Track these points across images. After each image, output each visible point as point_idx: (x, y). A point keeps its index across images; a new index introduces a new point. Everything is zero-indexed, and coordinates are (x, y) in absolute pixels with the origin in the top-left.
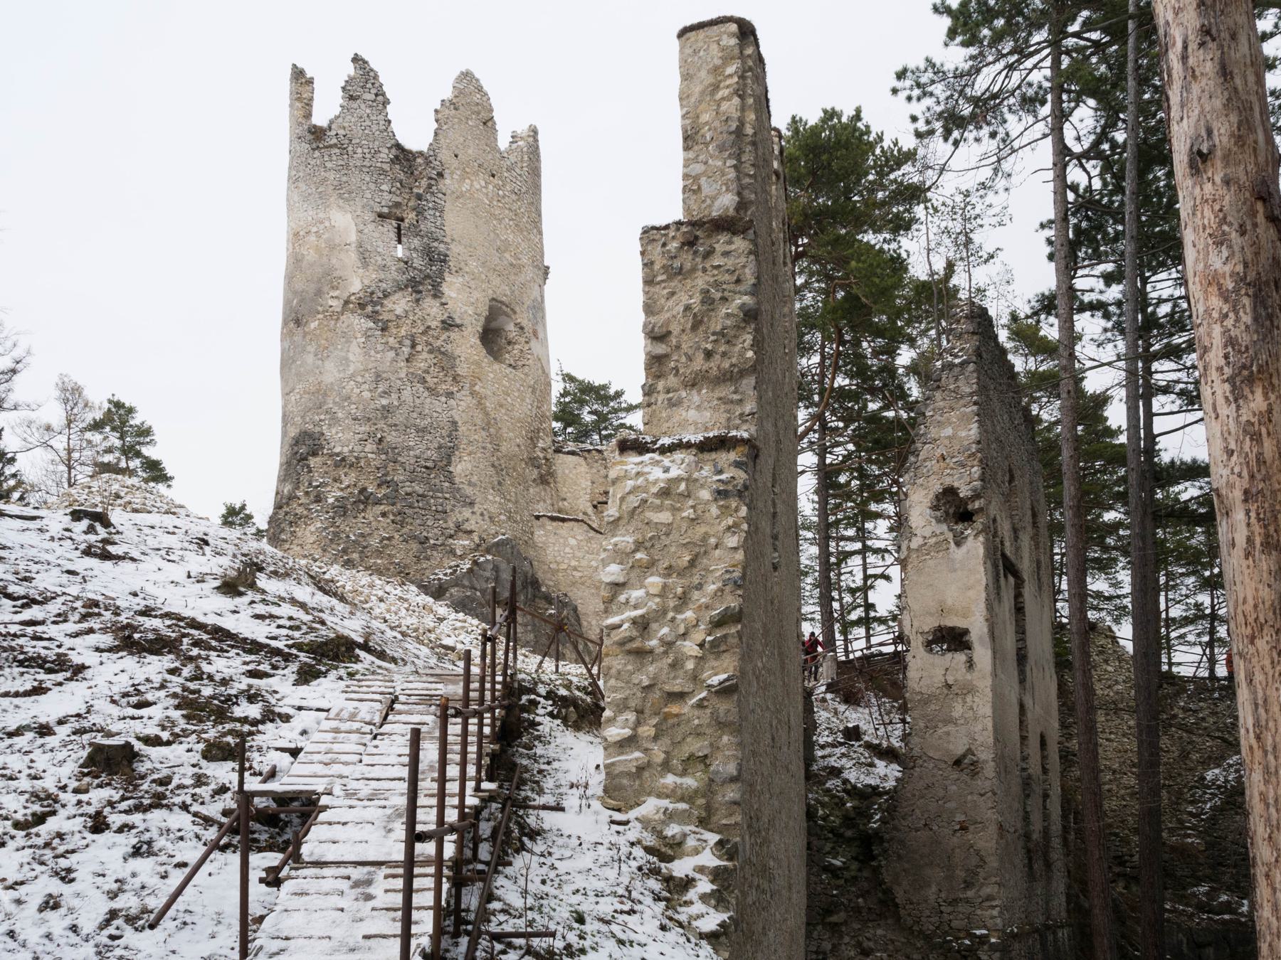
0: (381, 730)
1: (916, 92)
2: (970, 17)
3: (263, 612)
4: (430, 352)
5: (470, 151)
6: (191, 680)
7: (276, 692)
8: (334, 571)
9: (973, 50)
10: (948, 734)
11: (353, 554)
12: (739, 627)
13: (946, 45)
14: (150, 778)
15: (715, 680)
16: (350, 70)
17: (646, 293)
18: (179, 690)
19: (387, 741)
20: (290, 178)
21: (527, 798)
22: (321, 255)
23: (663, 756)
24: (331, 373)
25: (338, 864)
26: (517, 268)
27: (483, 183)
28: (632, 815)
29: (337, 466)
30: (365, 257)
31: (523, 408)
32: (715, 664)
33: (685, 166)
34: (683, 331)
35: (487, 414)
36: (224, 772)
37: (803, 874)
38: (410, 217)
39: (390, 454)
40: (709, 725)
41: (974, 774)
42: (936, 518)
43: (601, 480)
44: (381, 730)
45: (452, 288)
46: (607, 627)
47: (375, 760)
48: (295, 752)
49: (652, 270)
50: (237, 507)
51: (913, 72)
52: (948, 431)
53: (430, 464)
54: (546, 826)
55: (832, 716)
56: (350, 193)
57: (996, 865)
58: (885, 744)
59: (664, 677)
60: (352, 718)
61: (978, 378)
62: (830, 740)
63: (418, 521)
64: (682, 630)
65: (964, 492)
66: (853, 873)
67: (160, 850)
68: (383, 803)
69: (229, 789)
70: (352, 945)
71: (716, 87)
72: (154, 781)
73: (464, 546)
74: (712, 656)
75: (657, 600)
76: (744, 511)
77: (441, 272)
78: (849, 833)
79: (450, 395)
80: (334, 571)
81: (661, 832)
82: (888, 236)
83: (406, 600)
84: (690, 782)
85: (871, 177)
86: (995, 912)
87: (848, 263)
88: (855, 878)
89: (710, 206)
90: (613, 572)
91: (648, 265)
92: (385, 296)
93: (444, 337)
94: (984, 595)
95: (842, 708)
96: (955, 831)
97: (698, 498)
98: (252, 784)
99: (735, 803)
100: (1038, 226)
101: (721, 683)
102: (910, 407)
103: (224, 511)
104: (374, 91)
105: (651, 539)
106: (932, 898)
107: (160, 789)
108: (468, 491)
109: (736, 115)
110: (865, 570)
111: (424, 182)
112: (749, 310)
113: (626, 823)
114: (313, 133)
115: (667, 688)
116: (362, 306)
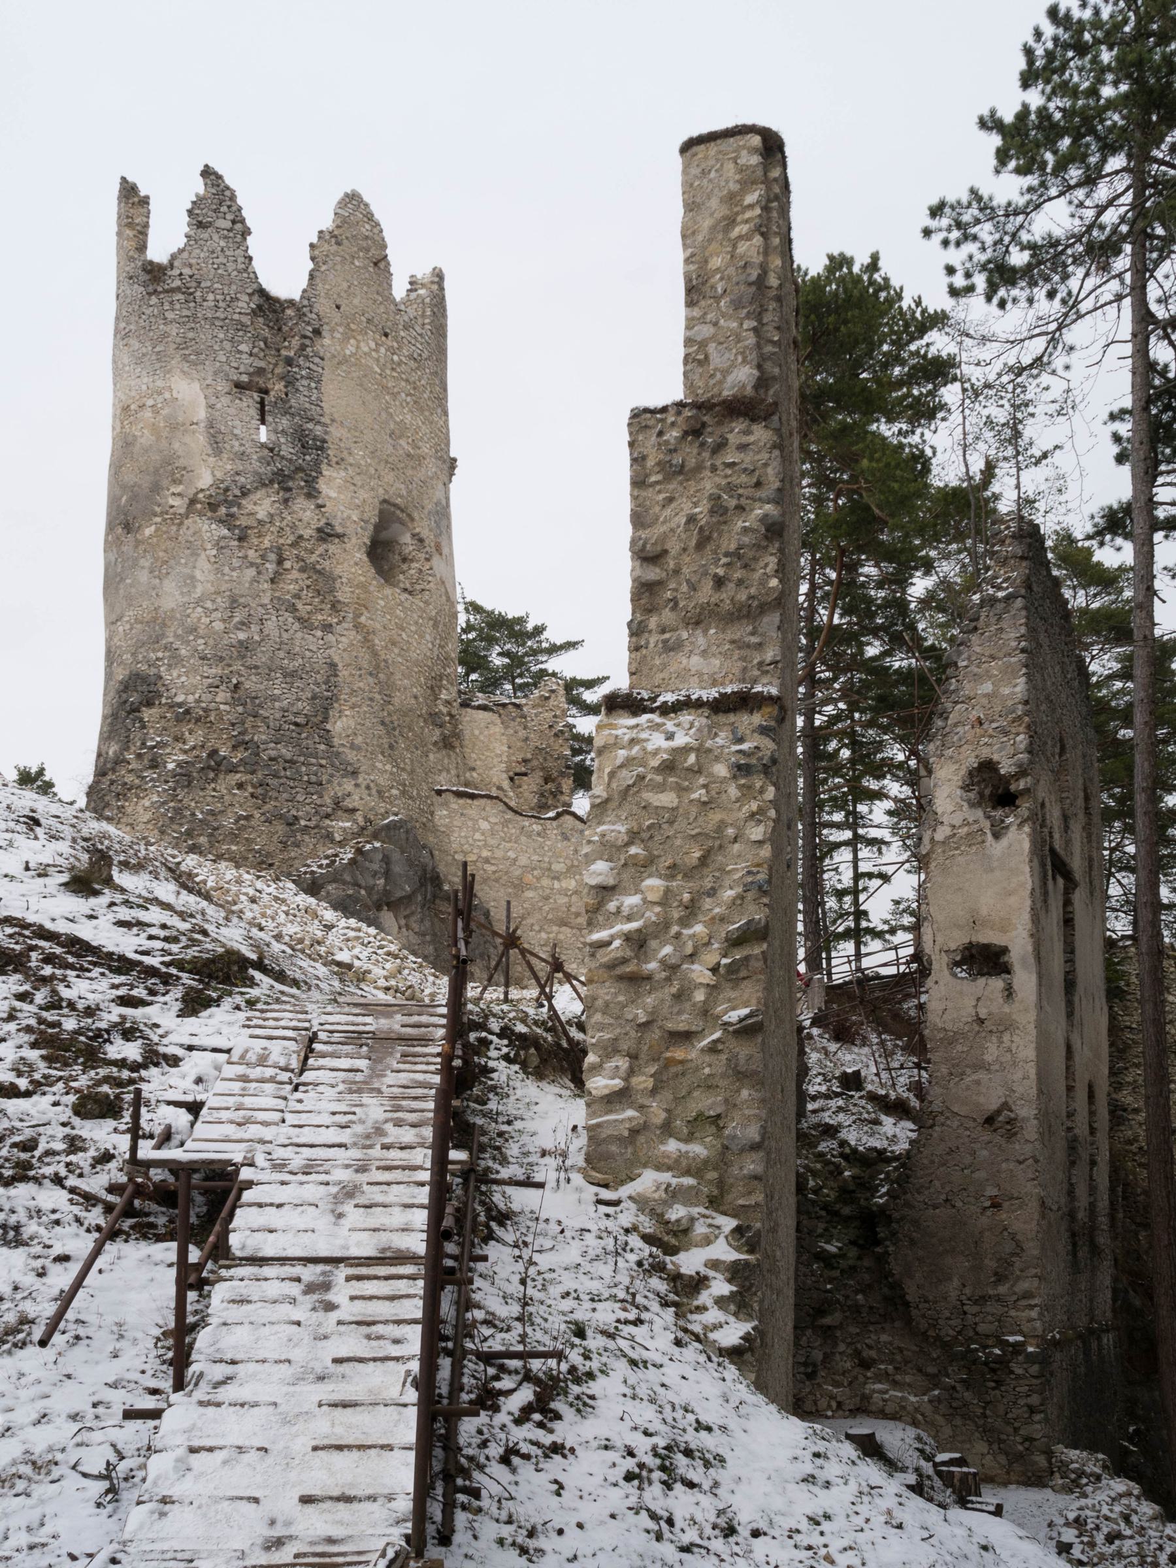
0: (303, 1079)
1: (955, 234)
2: (1027, 135)
3: (128, 918)
4: (302, 570)
5: (356, 301)
6: (47, 1008)
7: (157, 1026)
8: (190, 862)
9: (1032, 180)
10: (978, 1083)
11: (202, 836)
12: (765, 946)
13: (998, 172)
14: (9, 1142)
15: (733, 1016)
16: (198, 186)
17: (634, 498)
18: (33, 1022)
19: (312, 1094)
20: (117, 331)
21: (488, 1170)
22: (159, 438)
23: (663, 1115)
24: (171, 596)
25: (283, 1260)
26: (416, 459)
27: (373, 345)
28: (624, 1192)
29: (179, 719)
30: (216, 441)
31: (422, 646)
32: (733, 994)
33: (688, 328)
34: (685, 550)
35: (375, 654)
36: (104, 1134)
37: (792, 1259)
38: (278, 387)
39: (249, 706)
40: (724, 1076)
41: (1011, 1135)
42: (969, 801)
43: (519, 744)
44: (303, 1079)
45: (332, 484)
46: (591, 945)
47: (303, 1119)
48: (194, 1108)
49: (644, 467)
50: (33, 771)
51: (953, 208)
52: (987, 687)
54: (516, 1207)
55: (829, 1059)
56: (198, 354)
57: (1036, 1252)
58: (893, 1096)
59: (665, 1011)
60: (262, 1061)
61: (1027, 618)
62: (823, 1089)
63: (285, 795)
64: (689, 950)
65: (1006, 768)
66: (851, 1262)
67: (32, 1238)
68: (323, 1178)
69: (113, 1156)
70: (319, 1370)
71: (731, 222)
72: (14, 1145)
73: (344, 829)
74: (729, 985)
75: (658, 909)
76: (771, 793)
77: (317, 464)
78: (846, 1211)
79: (327, 628)
80: (190, 862)
81: (662, 1215)
82: (904, 427)
83: (284, 901)
84: (698, 1150)
85: (885, 348)
86: (1034, 1314)
87: (857, 461)
88: (853, 1268)
89: (721, 382)
90: (600, 871)
91: (638, 460)
92: (244, 494)
93: (320, 550)
94: (1028, 903)
95: (833, 1047)
96: (985, 1208)
97: (711, 775)
98: (146, 1151)
99: (756, 1178)
100: (1106, 416)
101: (741, 1020)
102: (932, 653)
104: (230, 217)
105: (649, 827)
106: (953, 1294)
107: (24, 1156)
108: (351, 756)
109: (757, 259)
110: (856, 867)
111: (296, 342)
112: (773, 524)
113: (616, 1203)
114: (149, 272)
115: (670, 1026)
116: (213, 507)
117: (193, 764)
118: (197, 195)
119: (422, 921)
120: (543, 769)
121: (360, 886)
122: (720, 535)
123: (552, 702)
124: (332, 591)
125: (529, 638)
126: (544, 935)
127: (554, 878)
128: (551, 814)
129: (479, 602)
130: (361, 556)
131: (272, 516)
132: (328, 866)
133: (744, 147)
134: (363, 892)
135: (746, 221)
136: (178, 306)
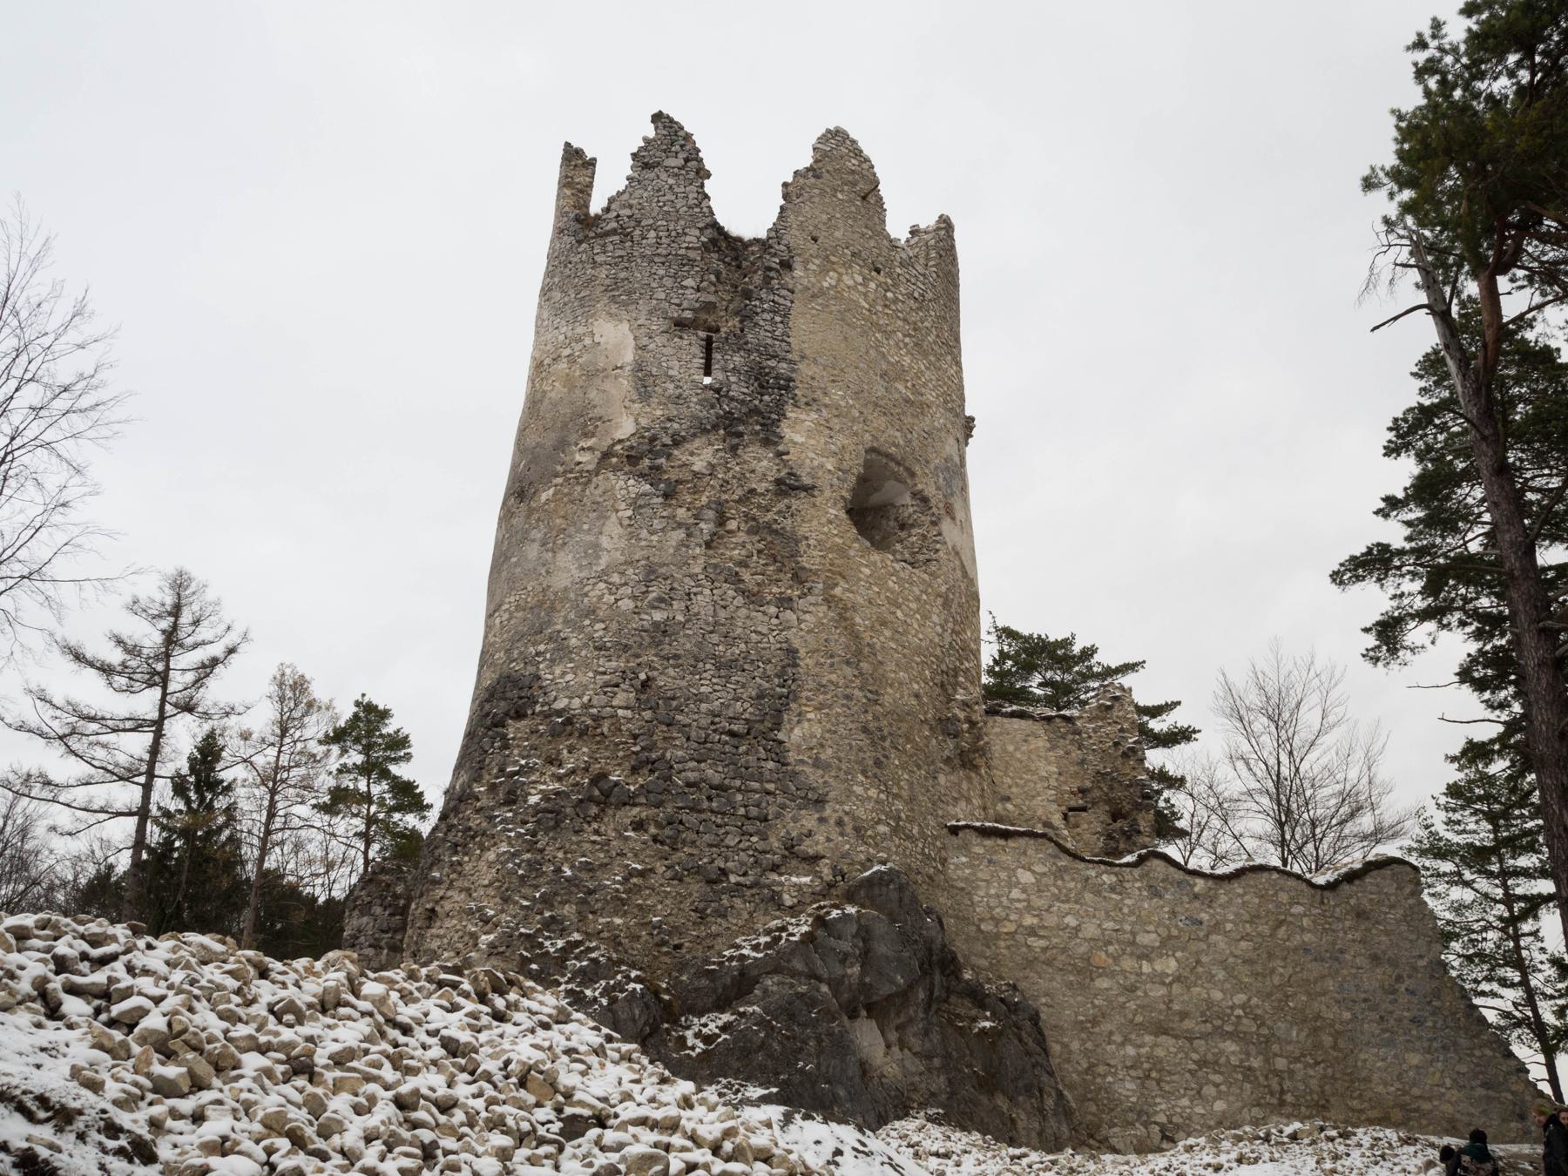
5: (837, 234)
24: (566, 570)
27: (859, 279)
29: (555, 734)
30: (644, 382)
35: (856, 636)
39: (662, 711)
45: (801, 432)
56: (629, 293)
73: (799, 887)
79: (784, 602)
92: (677, 443)
93: (781, 506)
104: (682, 155)
108: (814, 777)
116: (632, 459)
117: (566, 795)
118: (645, 139)
119: (926, 1033)
120: (1109, 801)
121: (819, 979)
123: (1115, 713)
124: (794, 555)
125: (1077, 664)
126: (1131, 1051)
127: (1140, 957)
128: (1129, 859)
129: (1014, 628)
130: (836, 512)
131: (712, 466)
132: (768, 946)
134: (824, 988)
136: (610, 248)
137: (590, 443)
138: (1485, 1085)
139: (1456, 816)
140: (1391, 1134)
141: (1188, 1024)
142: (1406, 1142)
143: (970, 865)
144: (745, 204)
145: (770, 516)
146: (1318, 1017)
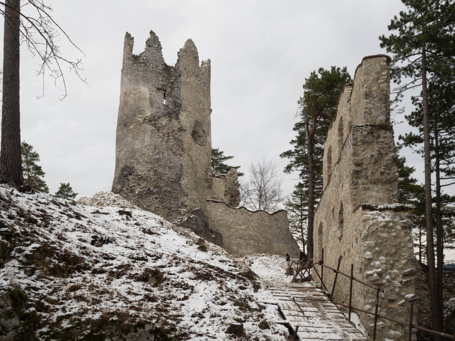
5: (190, 68)
16: (149, 36)
22: (135, 102)
24: (138, 145)
26: (204, 110)
27: (194, 79)
29: (139, 179)
30: (152, 103)
32: (406, 290)
35: (193, 163)
38: (169, 90)
45: (183, 116)
49: (356, 141)
53: (173, 180)
71: (378, 79)
73: (184, 211)
75: (385, 265)
77: (179, 110)
79: (181, 155)
89: (376, 119)
90: (368, 254)
92: (159, 118)
93: (179, 134)
97: (396, 229)
101: (412, 298)
103: (60, 186)
104: (158, 44)
105: (380, 242)
108: (186, 190)
111: (174, 78)
115: (390, 298)
116: (150, 121)
120: (231, 194)
122: (381, 160)
126: (236, 242)
130: (190, 136)
131: (166, 124)
133: (382, 60)
135: (383, 79)
137: (141, 116)
138: (292, 249)
139: (294, 198)
140: (278, 256)
141: (246, 237)
142: (280, 257)
143: (210, 207)
144: (170, 58)
145: (177, 136)
146: (267, 237)
